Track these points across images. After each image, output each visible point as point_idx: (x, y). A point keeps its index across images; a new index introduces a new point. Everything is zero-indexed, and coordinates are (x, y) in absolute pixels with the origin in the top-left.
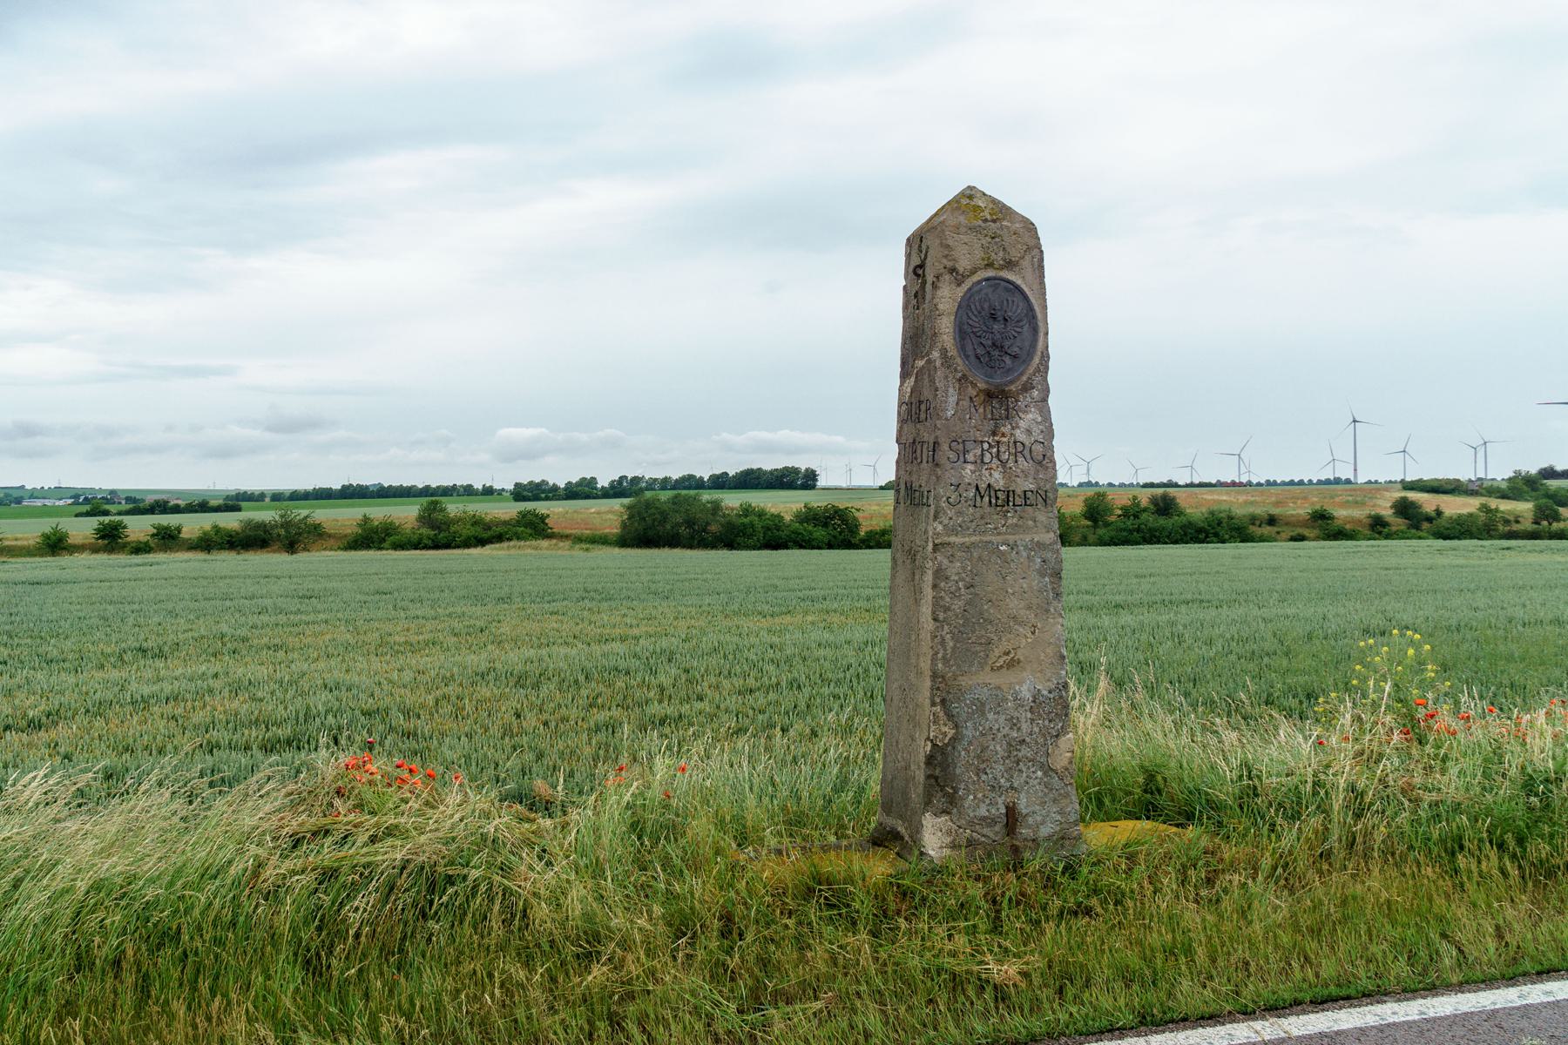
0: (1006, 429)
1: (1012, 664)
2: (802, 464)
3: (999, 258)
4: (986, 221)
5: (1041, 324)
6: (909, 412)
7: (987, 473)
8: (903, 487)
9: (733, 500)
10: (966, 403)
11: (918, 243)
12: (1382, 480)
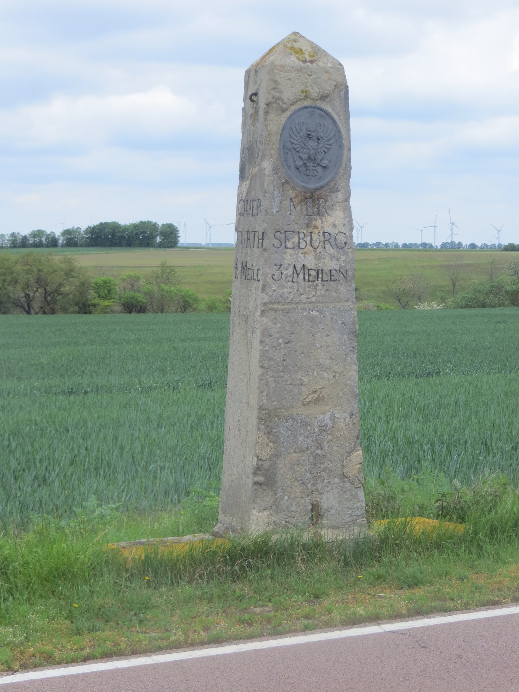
0: (318, 223)
1: (319, 400)
2: (160, 220)
3: (314, 92)
4: (305, 61)
5: (345, 142)
6: (246, 208)
7: (302, 256)
8: (240, 265)
9: (94, 263)
10: (287, 203)
11: (252, 75)
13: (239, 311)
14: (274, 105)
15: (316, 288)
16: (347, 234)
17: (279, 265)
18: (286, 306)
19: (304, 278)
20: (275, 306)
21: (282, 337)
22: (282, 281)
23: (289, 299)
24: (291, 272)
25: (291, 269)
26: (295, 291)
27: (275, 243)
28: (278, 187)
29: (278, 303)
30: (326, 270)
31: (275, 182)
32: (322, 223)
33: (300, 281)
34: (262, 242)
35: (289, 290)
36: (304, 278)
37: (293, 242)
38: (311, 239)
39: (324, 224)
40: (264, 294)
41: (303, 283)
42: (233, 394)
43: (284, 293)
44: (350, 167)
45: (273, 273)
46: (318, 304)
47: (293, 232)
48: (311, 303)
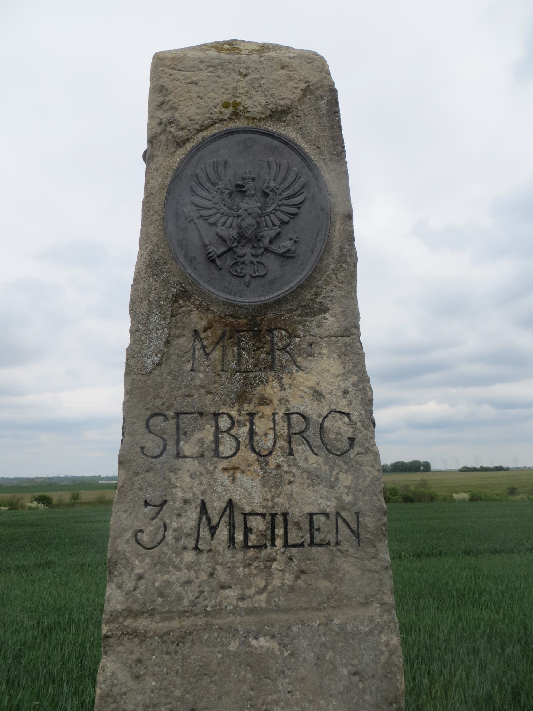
10: (184, 342)
18: (175, 624)
20: (143, 623)
26: (204, 576)
29: (152, 613)
35: (185, 574)
43: (168, 583)
45: (138, 525)
48: (251, 611)
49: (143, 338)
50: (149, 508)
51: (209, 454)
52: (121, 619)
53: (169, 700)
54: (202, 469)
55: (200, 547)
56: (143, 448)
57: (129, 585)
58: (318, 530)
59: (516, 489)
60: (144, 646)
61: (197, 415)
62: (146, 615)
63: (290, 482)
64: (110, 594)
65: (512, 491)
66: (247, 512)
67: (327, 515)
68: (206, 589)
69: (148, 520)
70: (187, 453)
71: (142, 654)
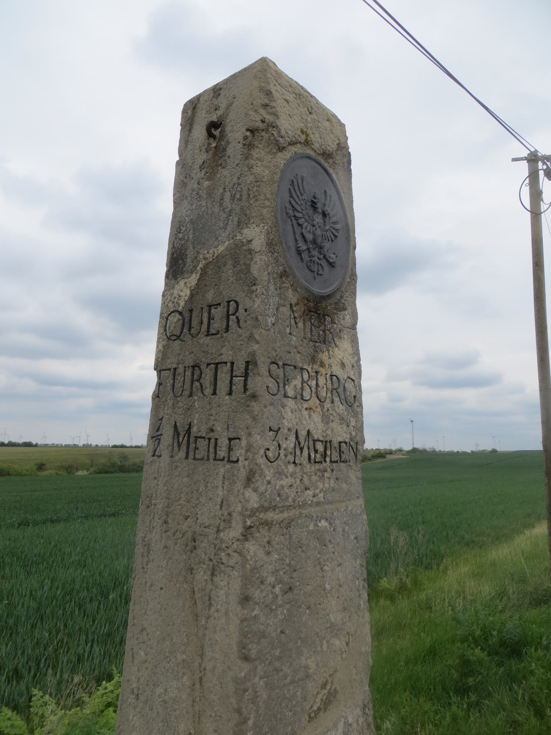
10: (285, 310)
12: (374, 449)
13: (166, 522)
14: (263, 134)
15: (323, 476)
16: (356, 380)
17: (276, 429)
18: (285, 515)
19: (309, 456)
20: (270, 516)
21: (280, 582)
22: (280, 463)
23: (290, 500)
24: (293, 445)
25: (293, 438)
26: (298, 481)
27: (270, 385)
28: (274, 278)
29: (274, 508)
30: (336, 441)
31: (270, 268)
32: (330, 358)
33: (305, 462)
34: (245, 381)
35: (290, 480)
36: (309, 456)
37: (295, 386)
38: (317, 385)
39: (332, 360)
40: (250, 490)
41: (308, 466)
42: (142, 698)
43: (282, 487)
44: (356, 276)
45: (267, 445)
46: (326, 506)
47: (295, 367)
48: (318, 504)
49: (266, 301)
50: (271, 432)
51: (299, 397)
52: (257, 514)
53: (284, 566)
54: (296, 407)
55: (296, 462)
56: (267, 387)
57: (262, 488)
58: (343, 452)
59: (44, 465)
60: (271, 531)
61: (293, 367)
62: (271, 509)
63: (333, 421)
64: (249, 496)
65: (41, 467)
66: (316, 439)
67: (346, 443)
68: (300, 490)
69: (271, 442)
70: (290, 395)
71: (270, 537)
